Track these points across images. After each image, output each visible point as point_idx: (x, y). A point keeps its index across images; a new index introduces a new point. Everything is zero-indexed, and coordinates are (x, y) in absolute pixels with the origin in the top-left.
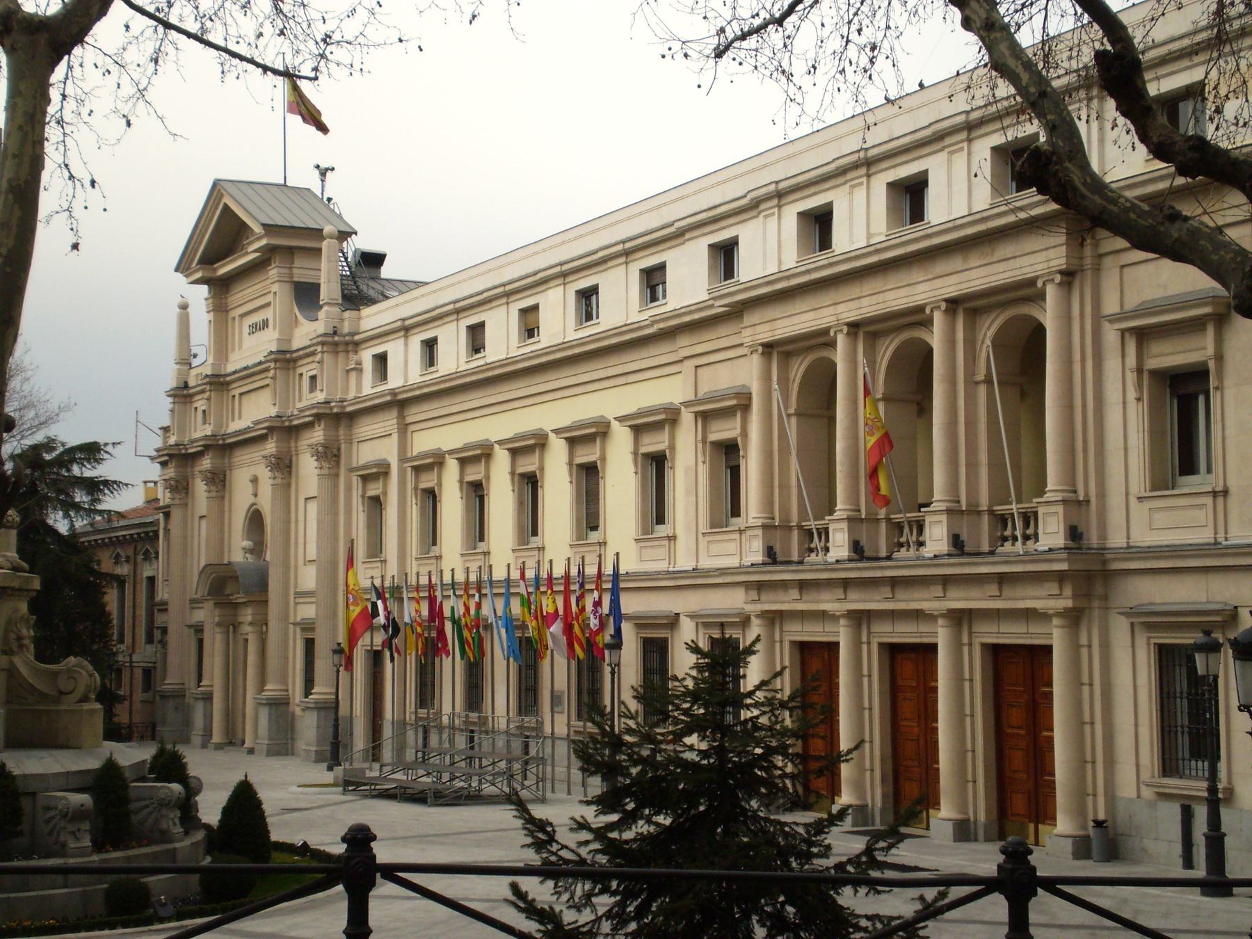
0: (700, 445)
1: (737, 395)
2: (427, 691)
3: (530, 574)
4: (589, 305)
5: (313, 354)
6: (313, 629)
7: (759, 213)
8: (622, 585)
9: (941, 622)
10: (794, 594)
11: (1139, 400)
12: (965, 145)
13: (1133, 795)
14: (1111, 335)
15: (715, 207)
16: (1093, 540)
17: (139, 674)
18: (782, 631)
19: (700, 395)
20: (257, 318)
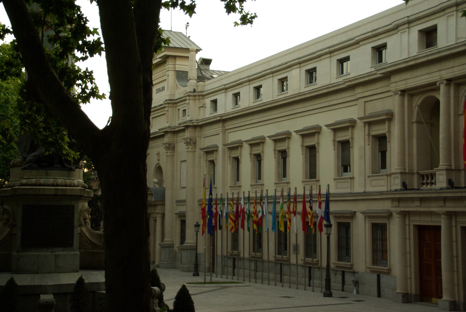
0: (367, 137)
1: (387, 114)
3: (285, 194)
4: (283, 86)
5: (185, 100)
6: (184, 216)
7: (398, 31)
8: (331, 199)
9: (443, 216)
10: (418, 203)
12: (455, 13)
15: (376, 30)
18: (409, 220)
19: (367, 114)
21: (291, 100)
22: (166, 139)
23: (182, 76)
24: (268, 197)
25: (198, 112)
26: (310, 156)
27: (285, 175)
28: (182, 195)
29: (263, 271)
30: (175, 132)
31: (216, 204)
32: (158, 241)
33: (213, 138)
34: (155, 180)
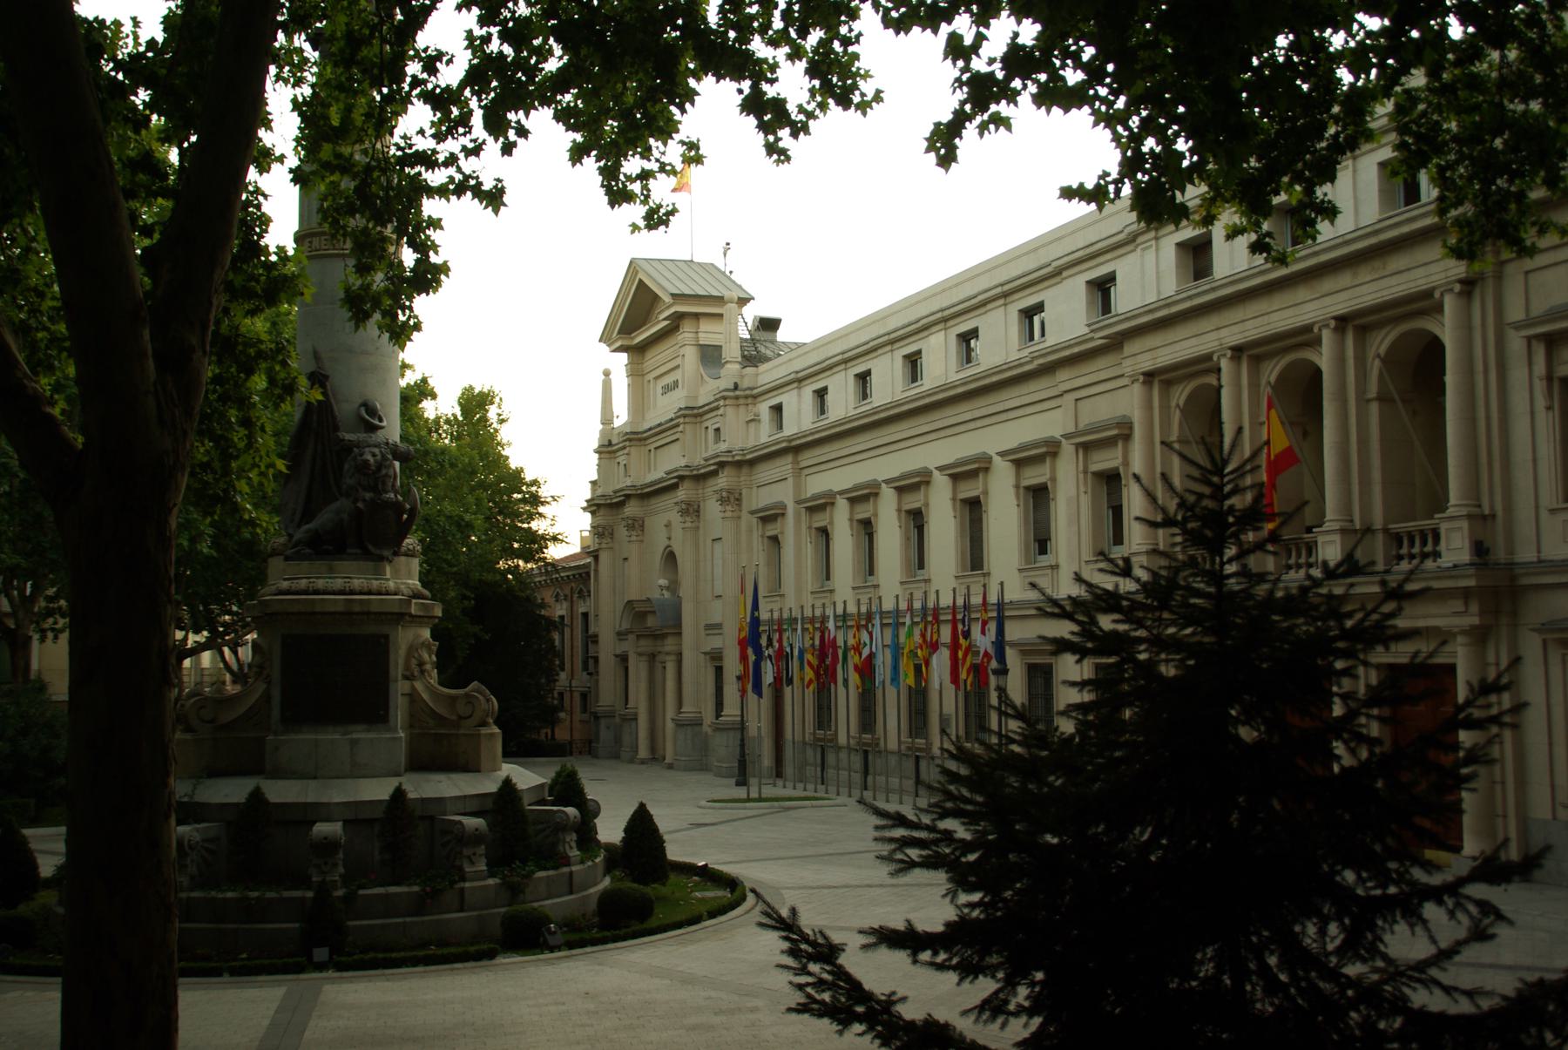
1: (1119, 425)
2: (824, 712)
3: (917, 605)
5: (717, 408)
6: (721, 659)
9: (1460, 639)
11: (1549, 408)
13: (1549, 816)
14: (1516, 343)
16: (1500, 555)
17: (577, 697)
19: (1081, 426)
20: (668, 380)
21: (927, 401)
22: (682, 494)
23: (711, 356)
24: (881, 613)
25: (744, 432)
26: (972, 521)
27: (921, 565)
28: (717, 613)
29: (838, 768)
30: (700, 478)
31: (781, 631)
32: (670, 713)
33: (775, 487)
34: (663, 582)
